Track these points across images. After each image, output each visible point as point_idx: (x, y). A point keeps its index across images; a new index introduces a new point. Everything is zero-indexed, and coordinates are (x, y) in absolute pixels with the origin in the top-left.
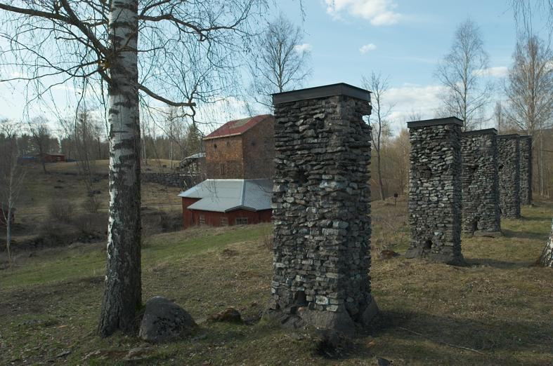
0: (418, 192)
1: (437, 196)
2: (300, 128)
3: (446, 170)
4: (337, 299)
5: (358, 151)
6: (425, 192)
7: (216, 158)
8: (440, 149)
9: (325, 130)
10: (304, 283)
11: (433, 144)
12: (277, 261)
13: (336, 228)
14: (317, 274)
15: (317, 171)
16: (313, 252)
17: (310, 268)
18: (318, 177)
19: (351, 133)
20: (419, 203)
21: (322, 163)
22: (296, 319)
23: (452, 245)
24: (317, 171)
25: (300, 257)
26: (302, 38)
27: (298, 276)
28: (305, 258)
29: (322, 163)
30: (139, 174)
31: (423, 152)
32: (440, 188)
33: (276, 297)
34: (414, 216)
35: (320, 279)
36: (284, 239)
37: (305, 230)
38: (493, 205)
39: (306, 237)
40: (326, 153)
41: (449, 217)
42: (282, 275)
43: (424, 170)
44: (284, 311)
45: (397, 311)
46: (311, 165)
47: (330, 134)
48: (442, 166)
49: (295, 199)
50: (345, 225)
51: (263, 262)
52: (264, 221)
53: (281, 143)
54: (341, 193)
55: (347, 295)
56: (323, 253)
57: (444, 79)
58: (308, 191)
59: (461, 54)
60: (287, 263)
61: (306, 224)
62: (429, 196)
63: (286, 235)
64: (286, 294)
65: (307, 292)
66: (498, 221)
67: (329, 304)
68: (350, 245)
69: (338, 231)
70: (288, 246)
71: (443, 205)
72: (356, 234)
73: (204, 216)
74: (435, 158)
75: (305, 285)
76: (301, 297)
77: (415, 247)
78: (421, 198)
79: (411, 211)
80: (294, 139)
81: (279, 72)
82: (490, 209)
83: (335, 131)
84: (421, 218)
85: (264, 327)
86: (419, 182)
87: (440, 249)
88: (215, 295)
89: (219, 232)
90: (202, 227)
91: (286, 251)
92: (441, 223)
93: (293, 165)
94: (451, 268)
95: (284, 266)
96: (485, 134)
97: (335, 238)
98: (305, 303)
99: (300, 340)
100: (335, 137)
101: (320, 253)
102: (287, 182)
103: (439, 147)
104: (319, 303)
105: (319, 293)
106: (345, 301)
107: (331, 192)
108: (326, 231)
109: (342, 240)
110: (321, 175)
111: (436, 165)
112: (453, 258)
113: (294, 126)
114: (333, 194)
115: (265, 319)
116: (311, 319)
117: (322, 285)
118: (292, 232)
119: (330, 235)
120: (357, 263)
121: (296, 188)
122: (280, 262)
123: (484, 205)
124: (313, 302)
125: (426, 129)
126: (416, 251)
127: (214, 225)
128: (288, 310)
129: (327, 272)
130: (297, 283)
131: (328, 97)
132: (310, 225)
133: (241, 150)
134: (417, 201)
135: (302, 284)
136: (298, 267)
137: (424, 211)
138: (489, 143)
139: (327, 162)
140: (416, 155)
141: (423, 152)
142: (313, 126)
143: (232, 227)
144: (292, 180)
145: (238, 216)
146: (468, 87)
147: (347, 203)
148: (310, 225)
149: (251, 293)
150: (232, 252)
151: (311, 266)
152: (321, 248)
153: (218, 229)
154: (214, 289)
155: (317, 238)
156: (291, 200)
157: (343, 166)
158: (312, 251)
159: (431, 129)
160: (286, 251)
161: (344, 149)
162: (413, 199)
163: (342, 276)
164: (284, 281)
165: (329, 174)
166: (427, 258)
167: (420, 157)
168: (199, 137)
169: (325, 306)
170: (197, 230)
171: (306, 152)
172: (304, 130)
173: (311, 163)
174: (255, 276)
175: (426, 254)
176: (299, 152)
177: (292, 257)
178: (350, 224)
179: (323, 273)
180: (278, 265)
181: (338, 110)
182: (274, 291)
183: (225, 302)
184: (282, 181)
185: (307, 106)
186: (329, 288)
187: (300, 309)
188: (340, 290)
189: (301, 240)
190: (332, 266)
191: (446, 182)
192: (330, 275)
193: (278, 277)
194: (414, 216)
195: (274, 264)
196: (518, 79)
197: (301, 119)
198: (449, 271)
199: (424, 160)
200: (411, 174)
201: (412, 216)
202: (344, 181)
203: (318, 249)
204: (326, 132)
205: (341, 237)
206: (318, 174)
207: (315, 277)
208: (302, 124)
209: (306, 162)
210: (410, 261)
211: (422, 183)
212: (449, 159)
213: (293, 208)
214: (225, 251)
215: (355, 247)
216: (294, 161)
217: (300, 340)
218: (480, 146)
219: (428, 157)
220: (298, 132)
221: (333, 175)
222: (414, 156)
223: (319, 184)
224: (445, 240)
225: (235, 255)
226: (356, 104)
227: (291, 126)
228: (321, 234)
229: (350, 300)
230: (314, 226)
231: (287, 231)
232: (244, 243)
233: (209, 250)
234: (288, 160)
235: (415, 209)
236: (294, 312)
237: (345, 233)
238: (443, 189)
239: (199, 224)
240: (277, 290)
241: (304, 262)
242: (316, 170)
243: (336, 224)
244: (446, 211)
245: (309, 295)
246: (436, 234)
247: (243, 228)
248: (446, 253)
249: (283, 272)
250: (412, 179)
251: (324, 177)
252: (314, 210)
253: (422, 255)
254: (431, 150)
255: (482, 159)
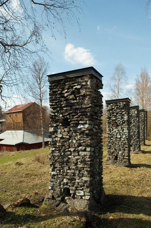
0: (111, 133)
1: (120, 135)
2: (65, 94)
3: (124, 123)
4: (89, 192)
5: (98, 108)
6: (114, 133)
7: (11, 121)
8: (121, 113)
9: (81, 95)
10: (68, 183)
11: (118, 111)
12: (52, 171)
13: (89, 152)
14: (77, 178)
15: (76, 119)
16: (74, 165)
17: (72, 174)
18: (77, 122)
19: (95, 98)
20: (111, 138)
21: (79, 114)
22: (64, 204)
23: (128, 158)
24: (76, 119)
25: (66, 168)
26: (49, 67)
27: (65, 179)
28: (69, 169)
29: (79, 114)
30: (34, 217)
31: (113, 115)
32: (122, 131)
33: (52, 191)
34: (109, 145)
35: (79, 181)
36: (56, 158)
37: (69, 153)
38: (138, 140)
39: (69, 157)
40: (81, 108)
41: (126, 145)
42: (55, 179)
43: (114, 123)
44: (57, 199)
45: (114, 194)
46: (72, 115)
47: (84, 97)
48: (122, 121)
49: (63, 135)
50: (93, 149)
51: (35, 168)
52: (33, 149)
53: (54, 104)
54: (91, 131)
55: (93, 189)
56: (80, 166)
57: (110, 88)
58: (71, 131)
59: (117, 77)
60: (58, 172)
61: (69, 150)
62: (116, 135)
63: (58, 156)
64: (58, 189)
65: (71, 188)
66: (139, 147)
67: (84, 195)
68: (95, 161)
69: (89, 153)
70: (58, 162)
71: (123, 139)
72: (97, 155)
73: (5, 147)
74: (119, 117)
75: (69, 184)
76: (67, 192)
77: (110, 159)
78: (113, 136)
79: (108, 142)
80: (61, 101)
81: (39, 82)
82: (137, 142)
83: (87, 95)
84: (113, 146)
85: (46, 209)
86: (111, 129)
87: (122, 160)
88: (14, 188)
89: (13, 154)
90: (5, 152)
91: (57, 165)
92: (122, 148)
93: (61, 116)
94: (129, 169)
95: (56, 174)
96: (134, 109)
97: (88, 157)
98: (69, 195)
99: (73, 221)
100: (87, 99)
101: (78, 166)
102: (57, 126)
103: (121, 112)
104: (78, 194)
105: (78, 189)
106: (93, 192)
107: (85, 131)
108: (82, 153)
109: (91, 158)
110: (78, 121)
111: (119, 121)
112: (128, 164)
113: (61, 93)
114: (86, 132)
115: (46, 204)
116: (74, 204)
117: (80, 184)
118: (61, 154)
119: (85, 155)
120: (98, 171)
121: (63, 129)
122: (54, 171)
123: (134, 140)
124: (75, 194)
125: (114, 104)
126: (110, 161)
127: (10, 151)
128: (60, 199)
129: (82, 177)
130: (64, 183)
131: (82, 76)
132: (72, 150)
133: (22, 117)
134: (111, 138)
135: (67, 183)
136: (65, 174)
137: (114, 142)
138: (136, 112)
139: (82, 114)
140: (110, 116)
141: (113, 115)
142: (73, 93)
143: (19, 152)
144: (61, 124)
145: (21, 146)
146: (119, 91)
147: (94, 137)
148: (72, 150)
149: (33, 186)
150: (20, 163)
151: (73, 173)
152: (79, 163)
153: (12, 152)
154: (12, 184)
155: (76, 157)
156: (60, 136)
157: (91, 115)
158: (74, 165)
159: (117, 104)
160: (57, 165)
161: (92, 105)
162: (109, 137)
163: (92, 178)
164: (56, 182)
165: (83, 120)
166: (116, 165)
167: (112, 117)
168: (2, 113)
169: (81, 196)
170: (2, 153)
171: (69, 108)
172: (67, 96)
173: (72, 114)
174: (33, 176)
175: (115, 162)
176: (65, 108)
177: (61, 169)
178: (95, 149)
179: (80, 177)
180: (53, 173)
181: (89, 83)
182: (50, 188)
183: (19, 191)
184: (55, 125)
185: (69, 82)
186: (84, 186)
187: (66, 198)
188: (91, 187)
189: (67, 158)
190: (86, 173)
191: (124, 129)
192: (84, 179)
193: (53, 180)
194: (109, 145)
195: (50, 172)
196: (138, 89)
197: (66, 89)
198: (128, 171)
199: (114, 118)
200: (107, 125)
201: (108, 145)
202: (92, 124)
203: (77, 164)
204: (82, 96)
205: (91, 157)
206: (76, 120)
207: (75, 180)
208: (67, 92)
209: (69, 114)
210: (108, 166)
211: (113, 129)
212: (126, 118)
213: (62, 140)
214: (17, 163)
215: (97, 162)
216: (62, 114)
217: (73, 221)
218: (132, 114)
219: (116, 117)
220: (64, 97)
221: (86, 121)
222: (109, 117)
223: (77, 127)
224: (124, 156)
225: (22, 165)
226: (97, 81)
227: (60, 94)
228: (79, 155)
229: (95, 192)
230: (74, 151)
231: (58, 154)
232: (25, 159)
233: (9, 163)
234: (58, 113)
235: (109, 142)
236: (63, 200)
237: (93, 153)
238: (123, 132)
239: (3, 151)
240: (52, 187)
241: (68, 171)
242: (75, 118)
243: (88, 149)
244: (124, 142)
245: (72, 190)
246: (120, 153)
247: (24, 152)
248: (125, 162)
249: (56, 177)
250: (108, 127)
251: (80, 122)
252: (74, 141)
253: (114, 163)
254: (117, 114)
255: (133, 119)
